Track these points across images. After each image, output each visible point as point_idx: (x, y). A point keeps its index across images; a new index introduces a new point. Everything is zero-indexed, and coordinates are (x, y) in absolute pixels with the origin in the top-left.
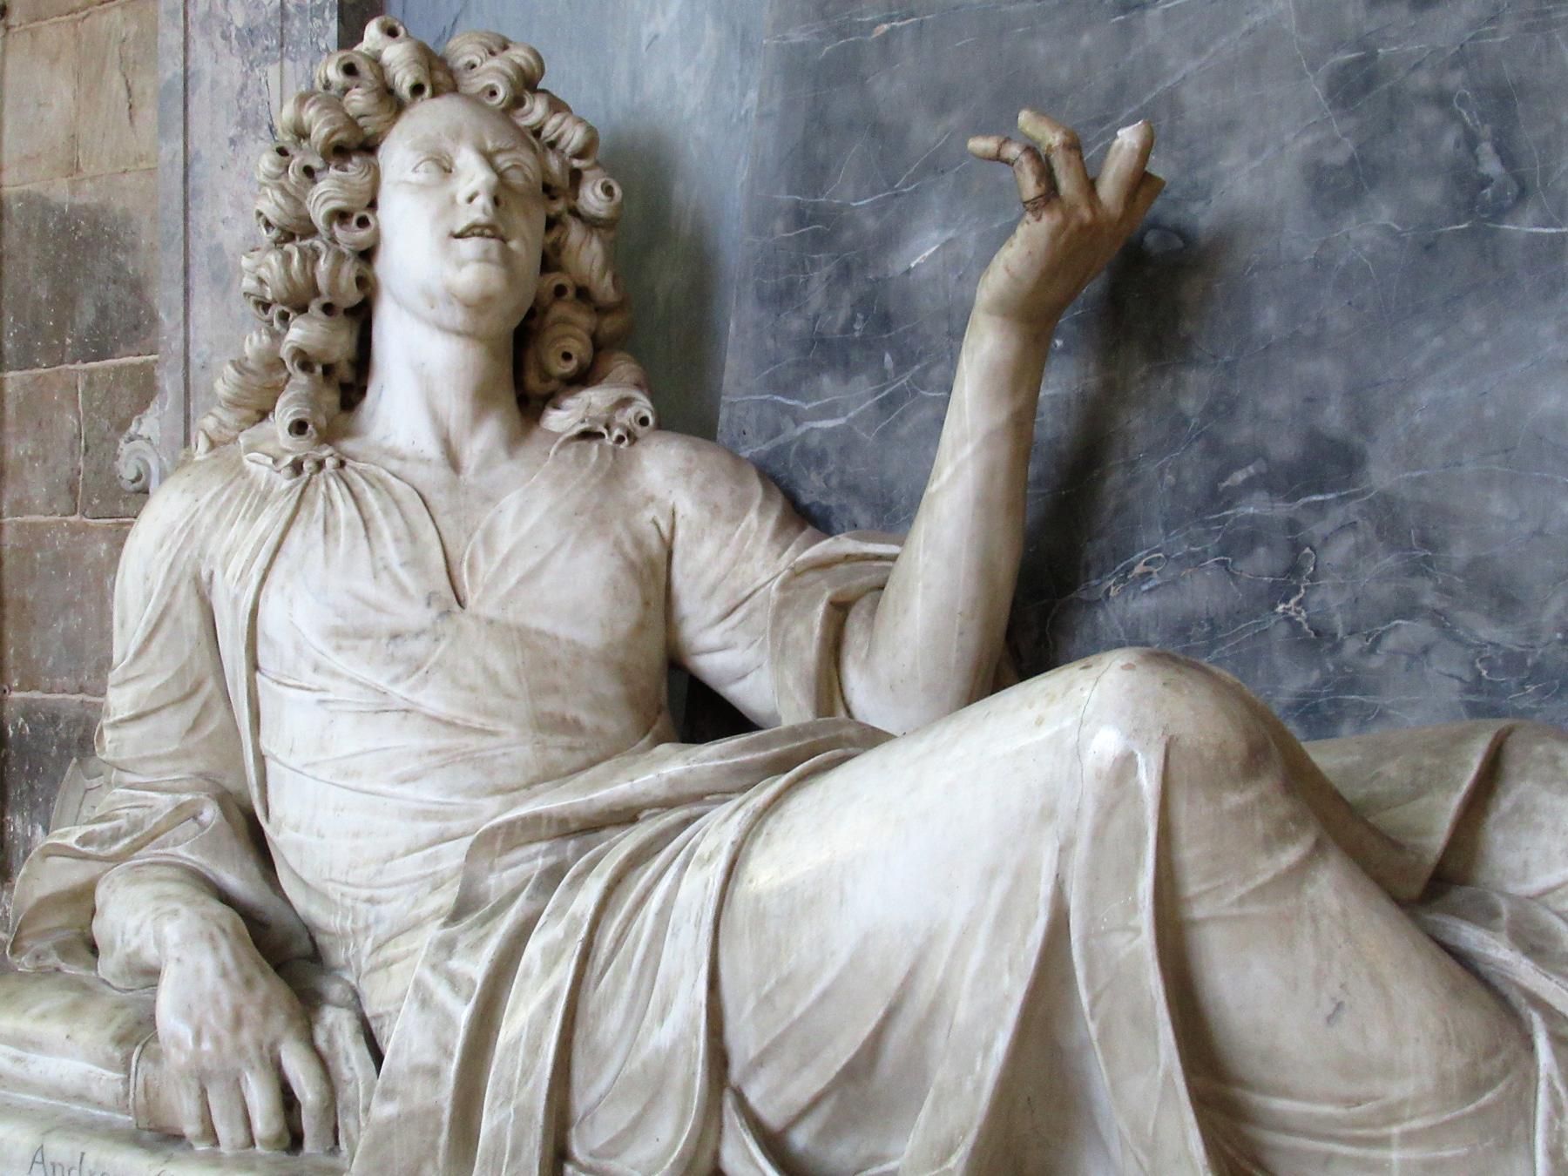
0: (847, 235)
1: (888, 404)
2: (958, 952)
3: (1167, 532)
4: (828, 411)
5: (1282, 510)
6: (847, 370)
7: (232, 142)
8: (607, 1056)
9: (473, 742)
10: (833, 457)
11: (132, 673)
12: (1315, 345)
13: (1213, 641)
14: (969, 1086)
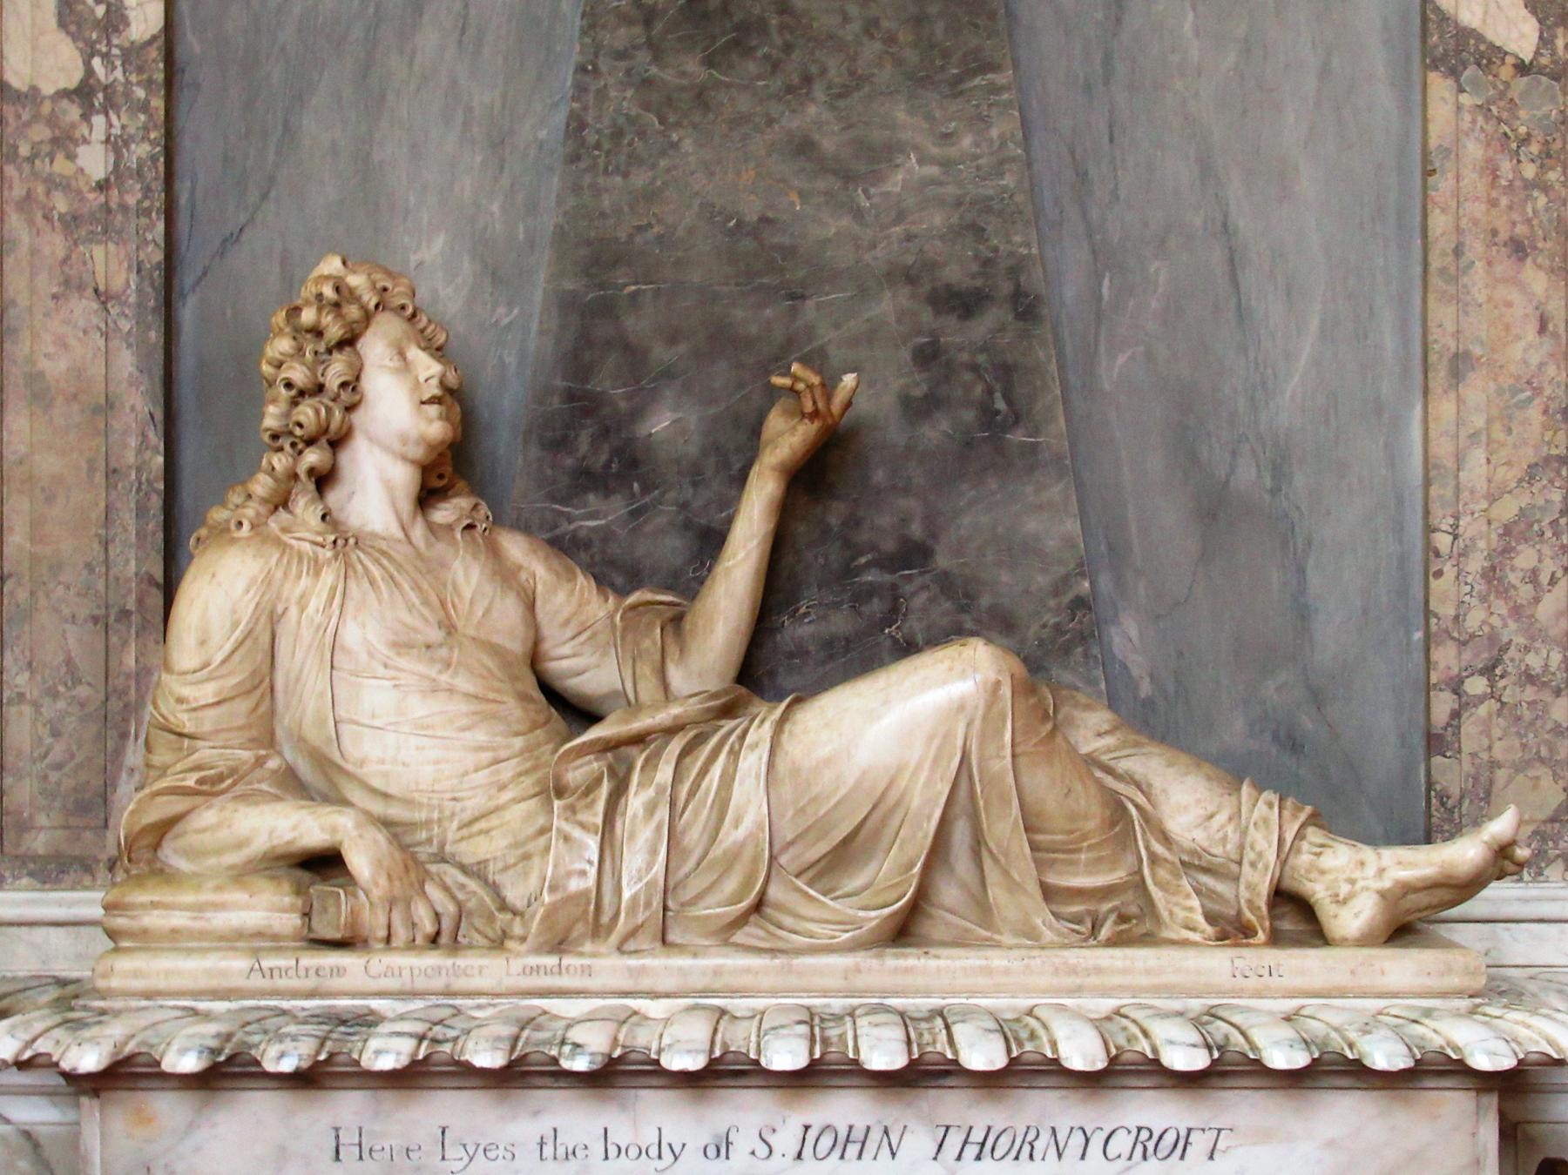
0: (606, 411)
1: (635, 514)
2: (915, 773)
3: (820, 589)
4: (593, 516)
5: (888, 578)
6: (607, 493)
7: (55, 297)
8: (690, 852)
9: (493, 707)
10: (597, 543)
11: (215, 674)
12: (906, 491)
13: (847, 649)
14: (920, 835)
